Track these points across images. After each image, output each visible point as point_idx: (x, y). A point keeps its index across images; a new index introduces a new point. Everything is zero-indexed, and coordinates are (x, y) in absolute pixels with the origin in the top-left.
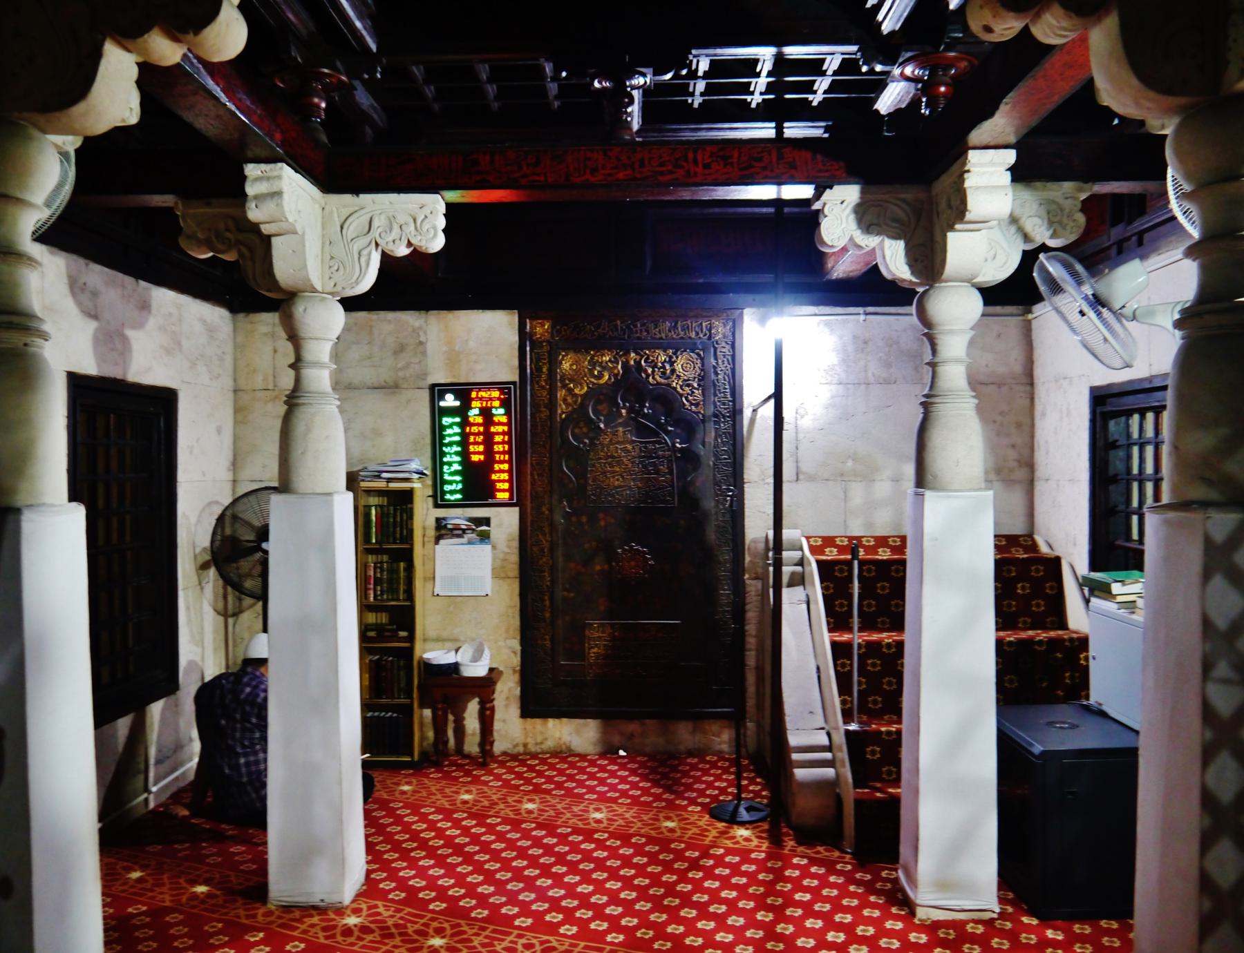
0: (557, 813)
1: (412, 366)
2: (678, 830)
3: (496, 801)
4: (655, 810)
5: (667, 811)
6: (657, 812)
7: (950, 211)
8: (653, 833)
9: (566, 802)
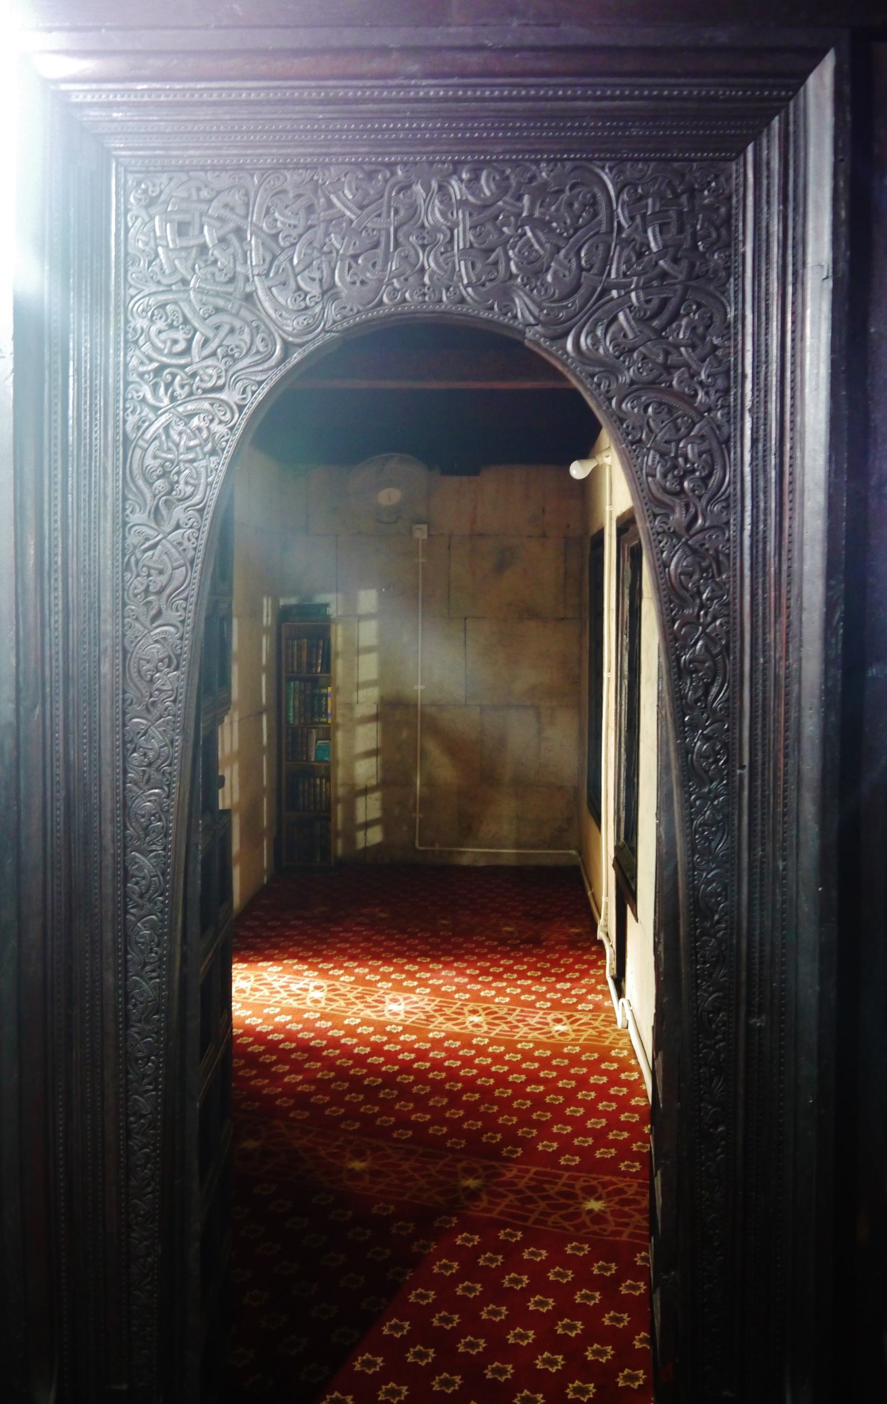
0: (348, 1004)
1: (527, 181)
2: (484, 1025)
3: (357, 1001)
4: (542, 1012)
5: (394, 993)
6: (544, 1014)
7: (667, 417)
8: (542, 1038)
9: (359, 990)
